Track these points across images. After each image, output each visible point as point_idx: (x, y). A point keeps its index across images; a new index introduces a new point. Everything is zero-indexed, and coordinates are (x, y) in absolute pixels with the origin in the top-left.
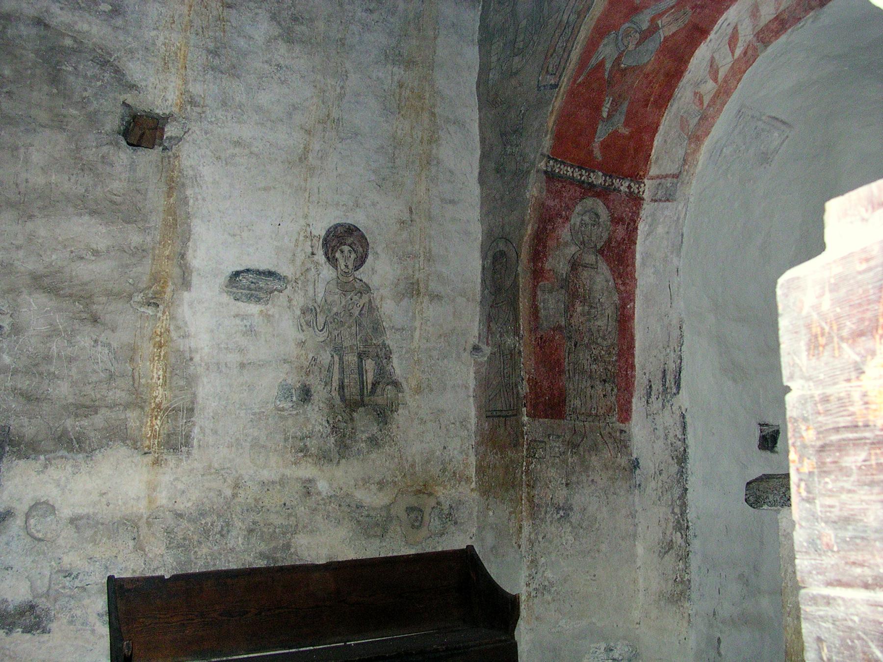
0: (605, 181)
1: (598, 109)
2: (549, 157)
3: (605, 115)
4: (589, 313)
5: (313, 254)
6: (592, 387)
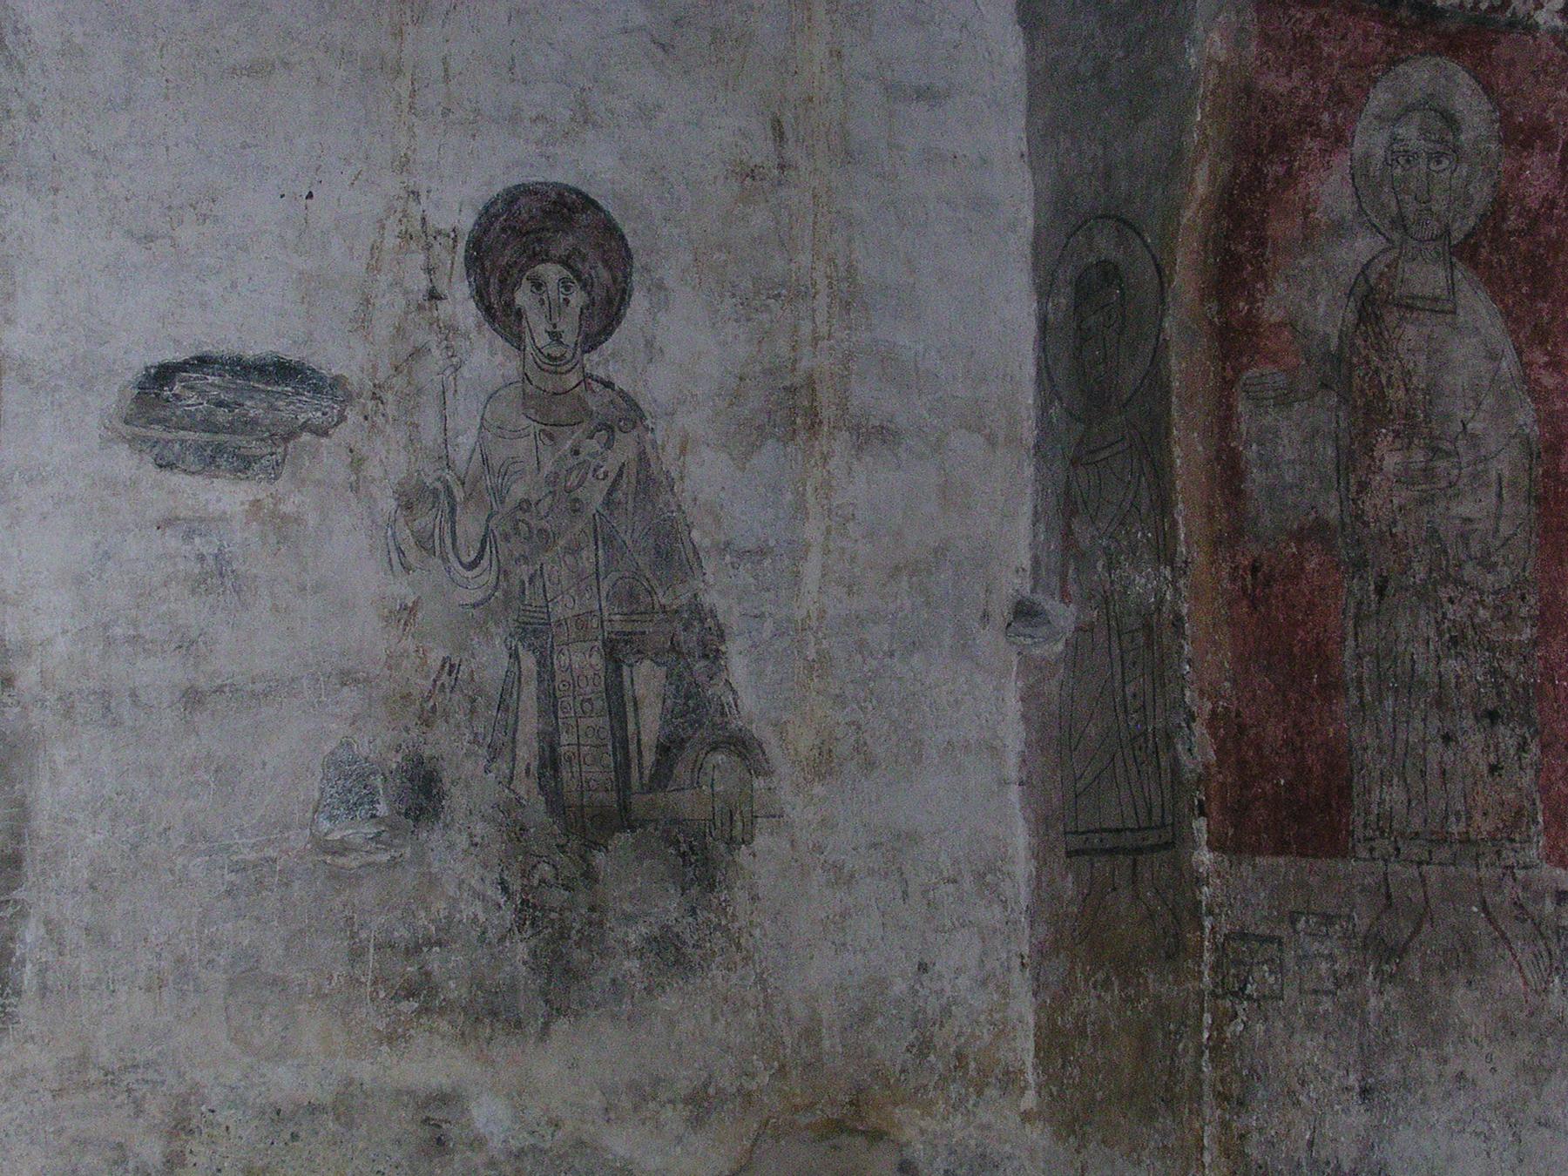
4: (1428, 473)
5: (433, 295)
6: (1447, 738)
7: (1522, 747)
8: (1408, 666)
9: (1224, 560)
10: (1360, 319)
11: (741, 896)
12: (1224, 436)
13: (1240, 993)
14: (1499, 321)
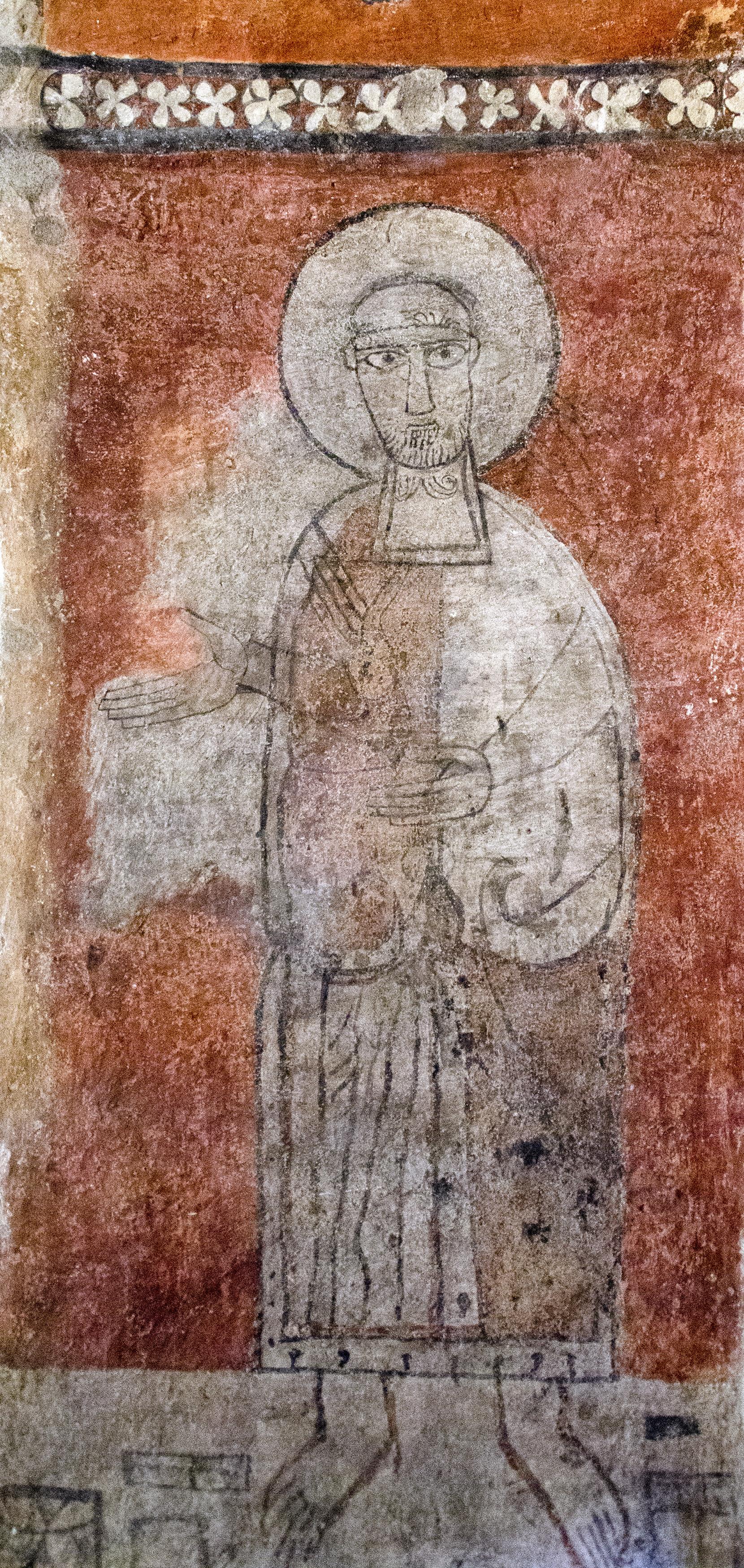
8: (379, 1083)
9: (44, 949)
10: (313, 588)
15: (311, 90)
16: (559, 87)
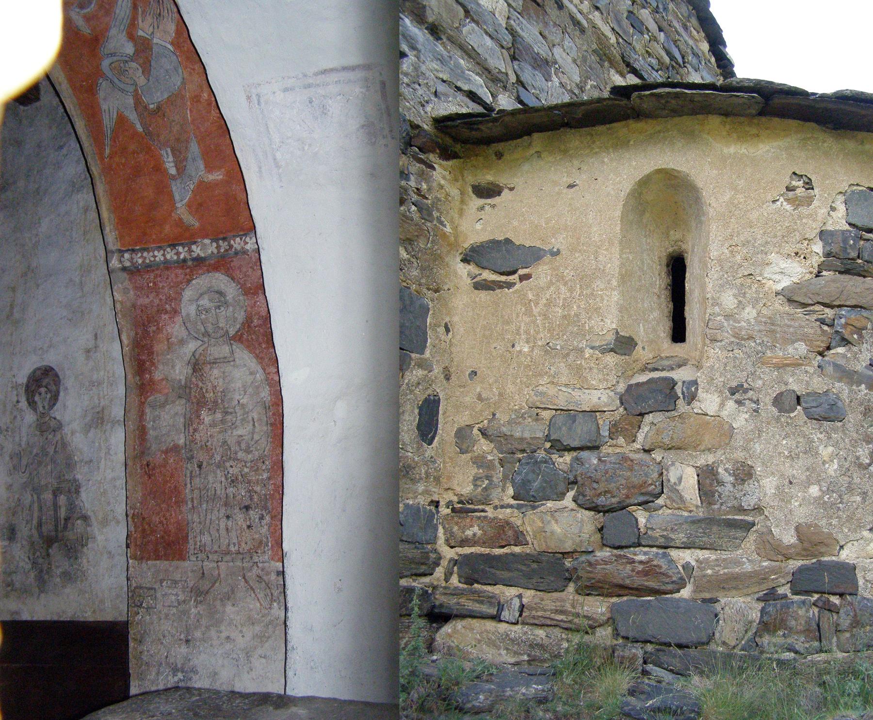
0: (218, 247)
1: (159, 168)
2: (120, 251)
3: (173, 171)
4: (223, 421)
5: (18, 402)
6: (228, 517)
7: (262, 518)
8: (213, 492)
11: (85, 561)
12: (140, 421)
13: (140, 606)
14: (254, 360)
15: (180, 249)
16: (238, 239)
